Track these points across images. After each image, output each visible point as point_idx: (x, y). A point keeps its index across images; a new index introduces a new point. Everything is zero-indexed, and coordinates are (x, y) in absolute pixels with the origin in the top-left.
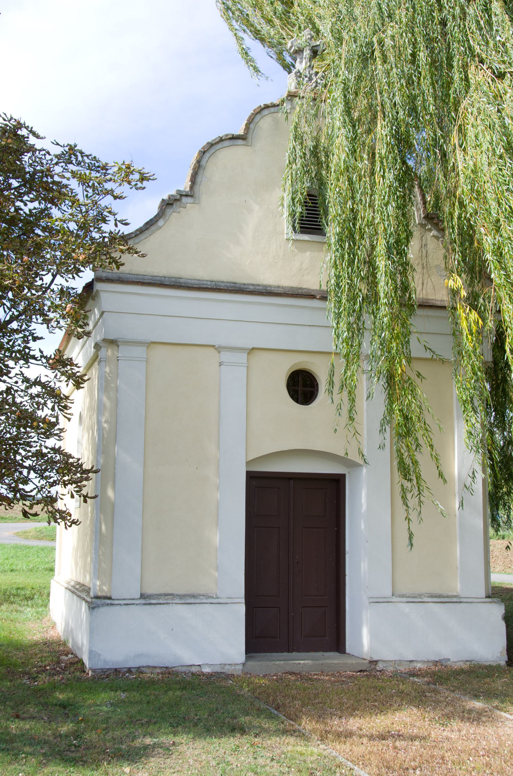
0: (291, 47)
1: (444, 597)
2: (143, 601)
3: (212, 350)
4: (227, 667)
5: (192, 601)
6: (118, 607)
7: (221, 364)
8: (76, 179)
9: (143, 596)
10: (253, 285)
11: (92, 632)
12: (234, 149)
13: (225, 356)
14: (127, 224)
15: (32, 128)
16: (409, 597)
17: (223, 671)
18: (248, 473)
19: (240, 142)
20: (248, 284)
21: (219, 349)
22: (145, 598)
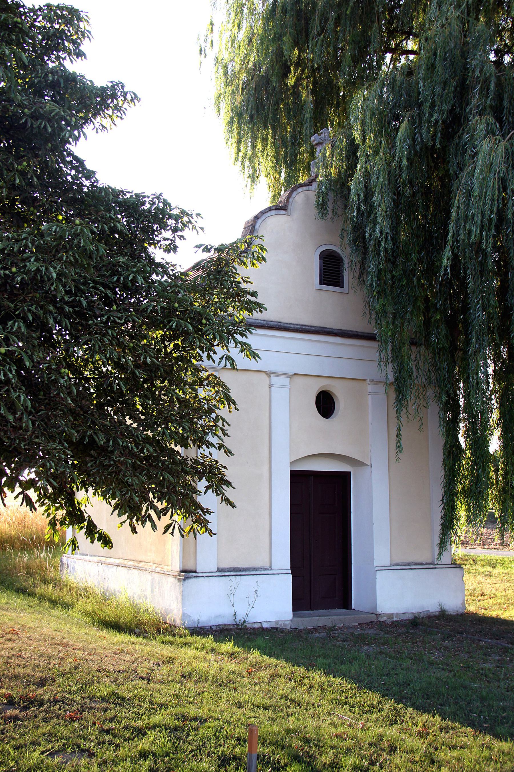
0: (314, 141)
1: (424, 565)
2: (219, 574)
3: (264, 374)
4: (280, 623)
5: (254, 573)
6: (202, 578)
7: (270, 386)
8: (82, 48)
9: (219, 570)
10: (293, 324)
11: (184, 598)
12: (278, 217)
13: (275, 380)
14: (255, 355)
15: (92, 542)
16: (401, 565)
17: (277, 626)
18: (292, 471)
19: (283, 212)
20: (290, 324)
21: (269, 374)
22: (220, 572)
